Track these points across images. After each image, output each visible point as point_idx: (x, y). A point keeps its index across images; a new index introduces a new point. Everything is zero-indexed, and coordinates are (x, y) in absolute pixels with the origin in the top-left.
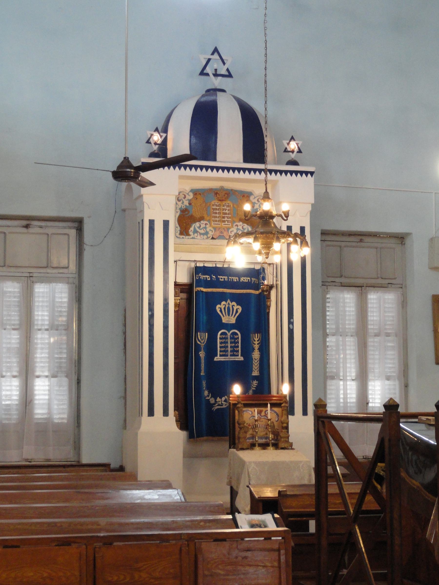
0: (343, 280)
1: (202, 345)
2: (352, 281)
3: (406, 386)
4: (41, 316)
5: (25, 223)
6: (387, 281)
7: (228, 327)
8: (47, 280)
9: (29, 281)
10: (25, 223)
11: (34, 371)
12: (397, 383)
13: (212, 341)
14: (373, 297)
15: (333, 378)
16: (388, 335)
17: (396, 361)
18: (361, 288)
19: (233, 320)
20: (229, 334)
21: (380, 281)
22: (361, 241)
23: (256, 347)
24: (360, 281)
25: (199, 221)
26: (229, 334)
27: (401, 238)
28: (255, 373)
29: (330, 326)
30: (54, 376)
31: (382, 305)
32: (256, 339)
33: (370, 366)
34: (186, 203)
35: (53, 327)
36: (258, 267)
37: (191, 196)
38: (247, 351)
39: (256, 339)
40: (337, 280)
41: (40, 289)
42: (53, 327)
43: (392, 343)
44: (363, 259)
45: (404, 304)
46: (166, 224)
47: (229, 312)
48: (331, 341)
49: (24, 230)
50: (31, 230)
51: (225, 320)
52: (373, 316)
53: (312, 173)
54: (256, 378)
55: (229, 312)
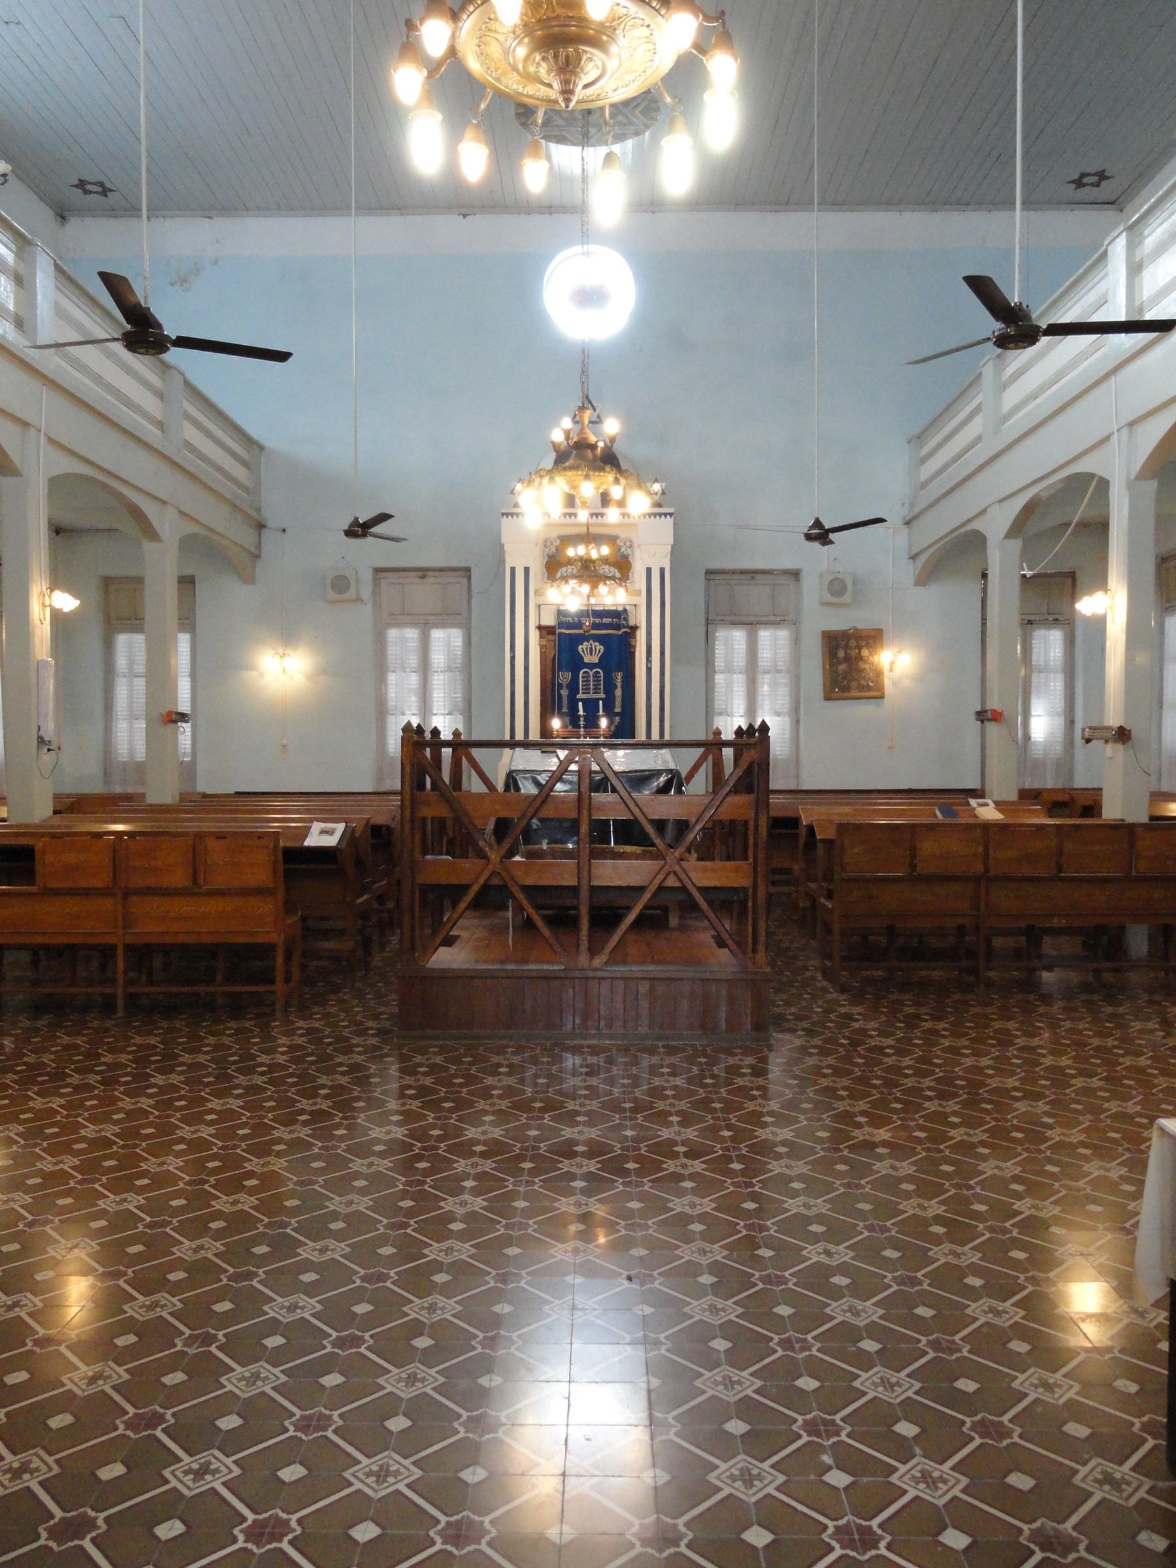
0: (734, 618)
1: (565, 684)
2: (745, 619)
3: (798, 722)
4: (438, 658)
5: (421, 574)
6: (779, 619)
7: (591, 666)
8: (443, 625)
9: (425, 629)
10: (421, 574)
11: (431, 710)
12: (787, 719)
13: (575, 679)
14: (765, 635)
15: (720, 714)
16: (779, 671)
17: (788, 698)
18: (751, 625)
19: (596, 660)
20: (591, 673)
21: (772, 618)
22: (753, 578)
23: (619, 684)
24: (751, 619)
25: (566, 565)
26: (591, 673)
27: (795, 574)
28: (618, 710)
29: (719, 663)
30: (449, 714)
31: (773, 643)
32: (619, 677)
33: (759, 703)
34: (554, 549)
35: (449, 669)
36: (620, 609)
37: (558, 542)
38: (609, 688)
39: (619, 677)
40: (727, 618)
41: (437, 634)
42: (449, 669)
43: (784, 679)
44: (756, 596)
45: (796, 640)
46: (662, 571)
47: (591, 652)
48: (719, 678)
49: (418, 580)
50: (426, 580)
51: (587, 659)
52: (765, 654)
53: (671, 515)
54: (617, 714)
55: (591, 652)
